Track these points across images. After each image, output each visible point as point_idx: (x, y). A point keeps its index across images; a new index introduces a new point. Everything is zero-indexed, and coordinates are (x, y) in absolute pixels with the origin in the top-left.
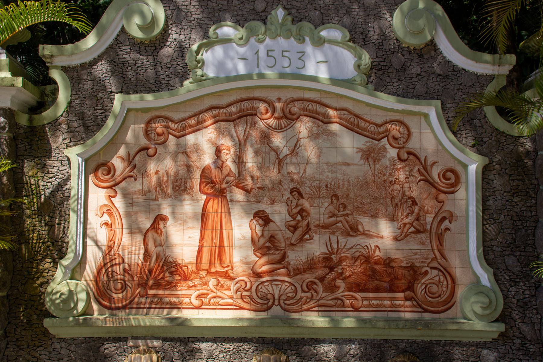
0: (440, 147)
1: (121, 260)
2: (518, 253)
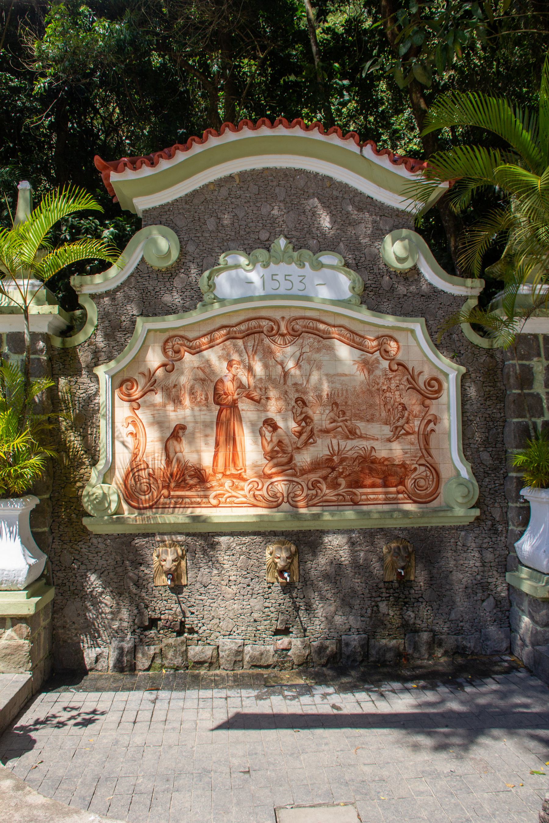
0: (425, 359)
1: (145, 465)
2: (490, 449)
